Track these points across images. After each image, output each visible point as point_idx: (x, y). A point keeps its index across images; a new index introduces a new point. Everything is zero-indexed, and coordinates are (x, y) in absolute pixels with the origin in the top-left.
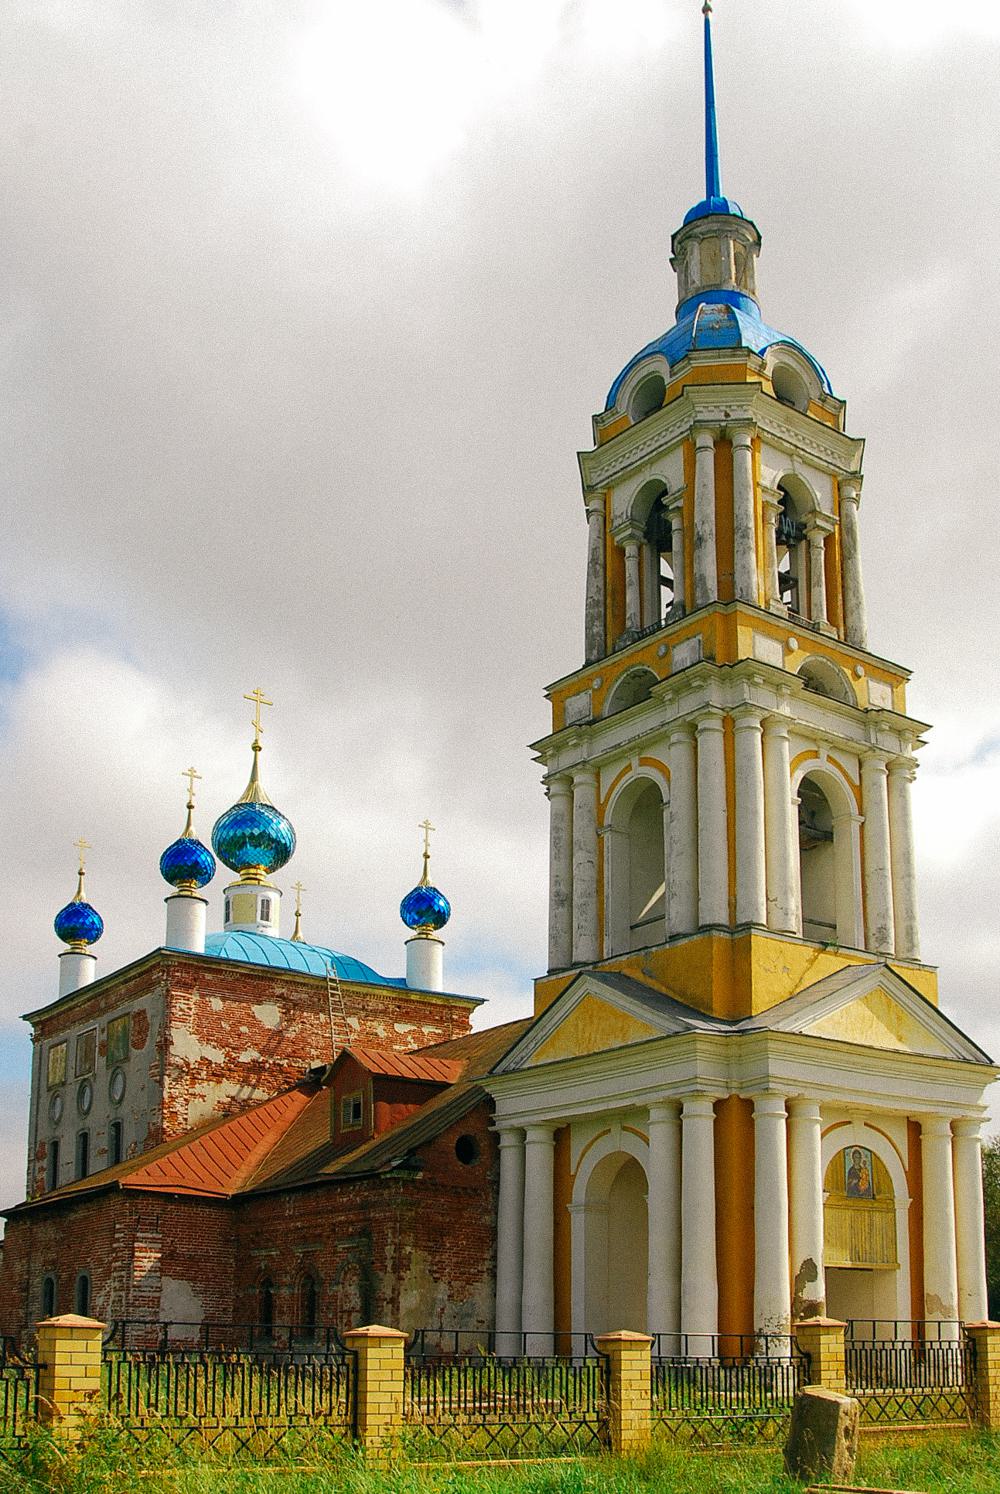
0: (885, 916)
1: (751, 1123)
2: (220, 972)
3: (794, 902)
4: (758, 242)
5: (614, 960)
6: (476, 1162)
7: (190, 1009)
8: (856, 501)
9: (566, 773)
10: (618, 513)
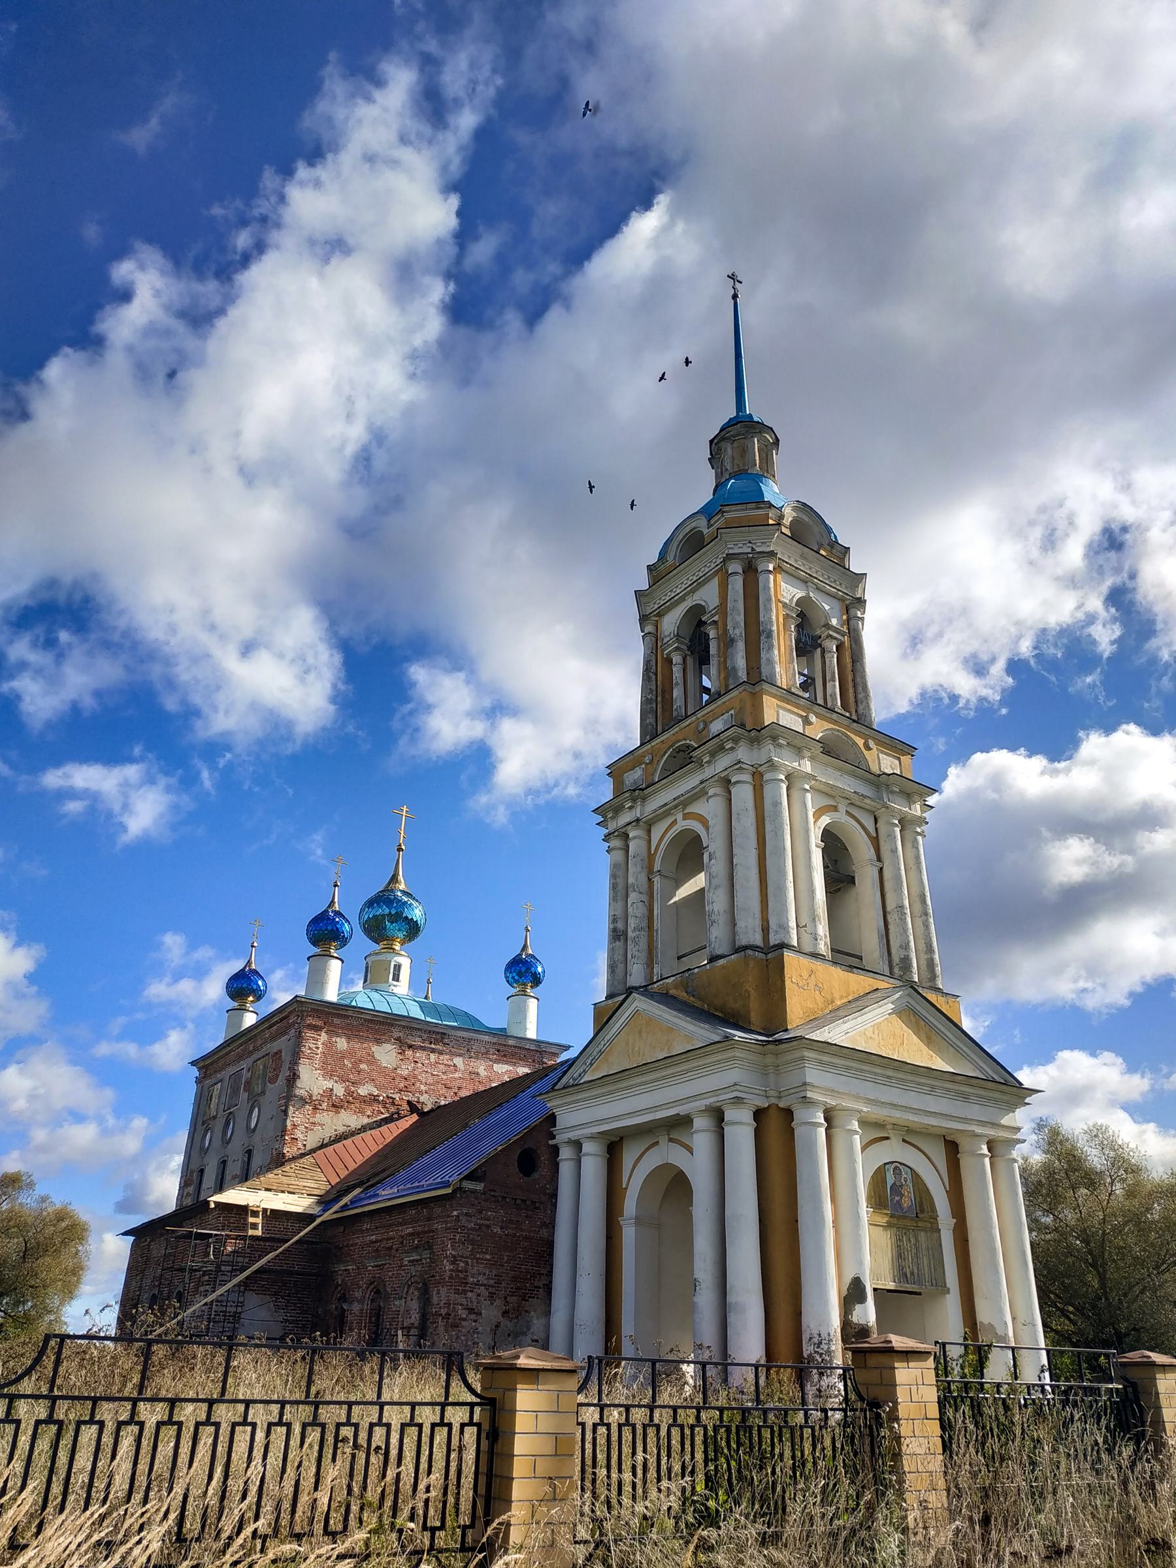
0: (906, 947)
1: (791, 1132)
2: (347, 1017)
3: (822, 929)
4: (777, 441)
5: (661, 982)
6: (536, 1175)
7: (318, 1048)
8: (862, 619)
9: (623, 830)
10: (667, 633)
